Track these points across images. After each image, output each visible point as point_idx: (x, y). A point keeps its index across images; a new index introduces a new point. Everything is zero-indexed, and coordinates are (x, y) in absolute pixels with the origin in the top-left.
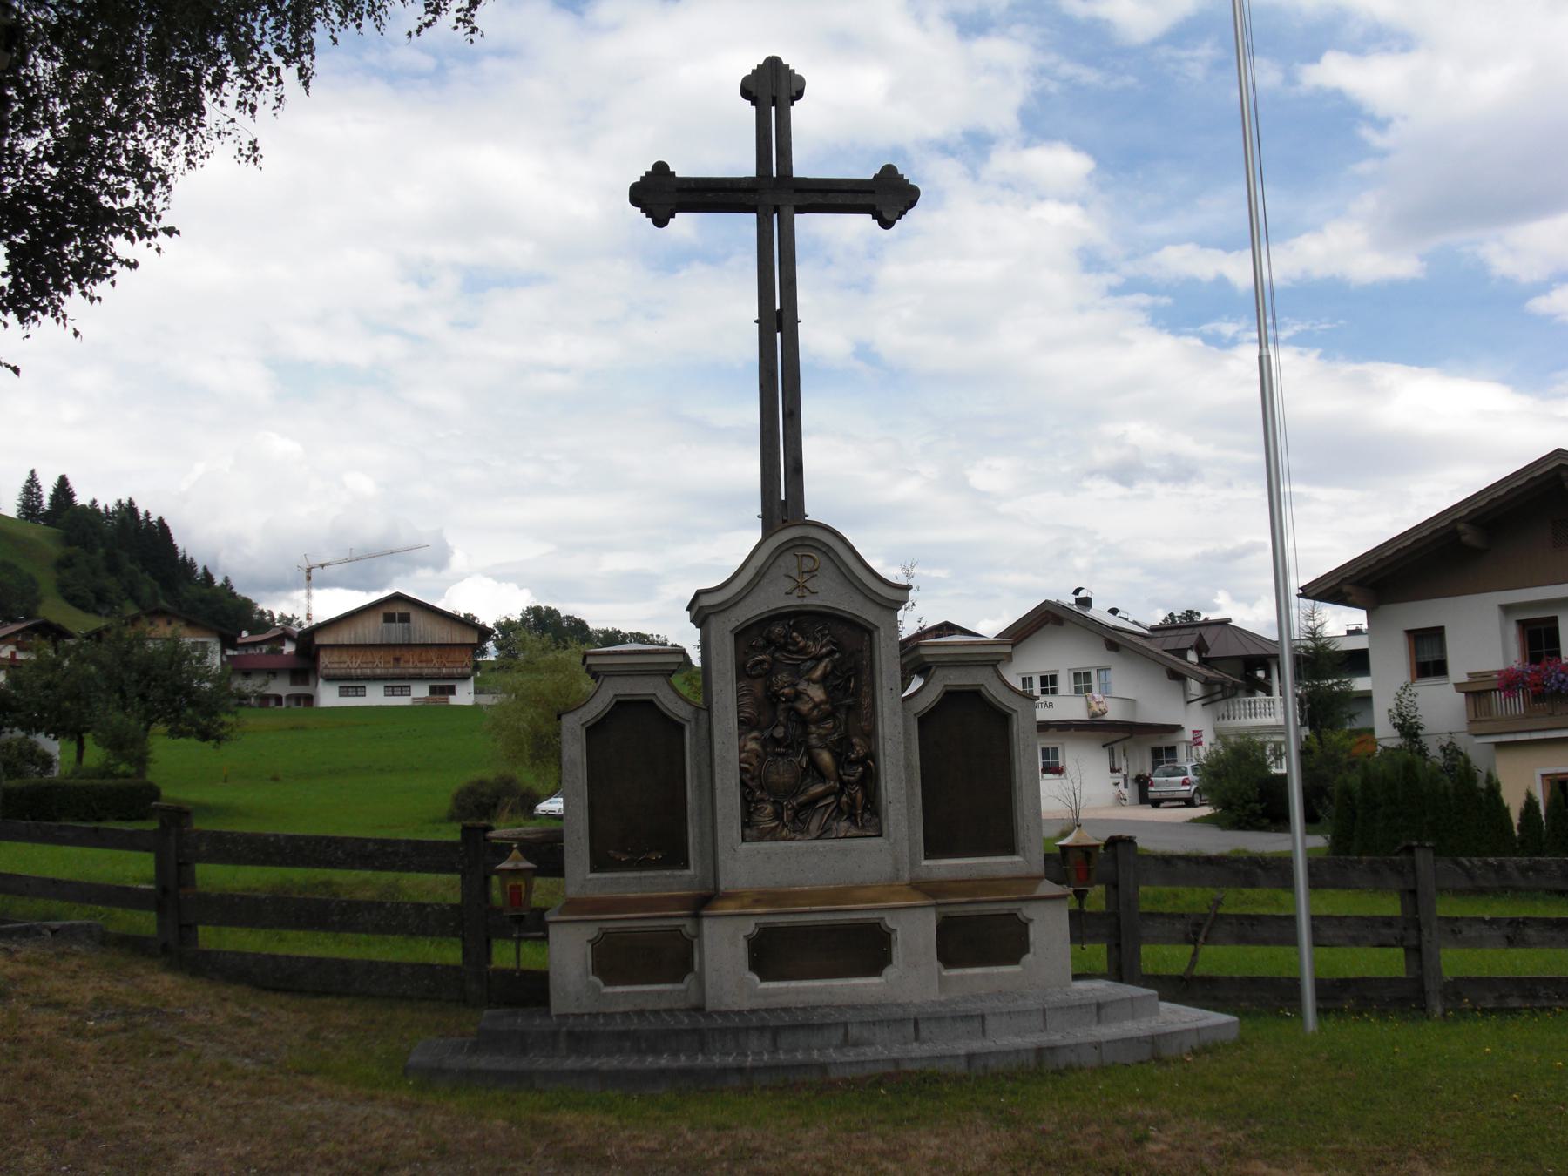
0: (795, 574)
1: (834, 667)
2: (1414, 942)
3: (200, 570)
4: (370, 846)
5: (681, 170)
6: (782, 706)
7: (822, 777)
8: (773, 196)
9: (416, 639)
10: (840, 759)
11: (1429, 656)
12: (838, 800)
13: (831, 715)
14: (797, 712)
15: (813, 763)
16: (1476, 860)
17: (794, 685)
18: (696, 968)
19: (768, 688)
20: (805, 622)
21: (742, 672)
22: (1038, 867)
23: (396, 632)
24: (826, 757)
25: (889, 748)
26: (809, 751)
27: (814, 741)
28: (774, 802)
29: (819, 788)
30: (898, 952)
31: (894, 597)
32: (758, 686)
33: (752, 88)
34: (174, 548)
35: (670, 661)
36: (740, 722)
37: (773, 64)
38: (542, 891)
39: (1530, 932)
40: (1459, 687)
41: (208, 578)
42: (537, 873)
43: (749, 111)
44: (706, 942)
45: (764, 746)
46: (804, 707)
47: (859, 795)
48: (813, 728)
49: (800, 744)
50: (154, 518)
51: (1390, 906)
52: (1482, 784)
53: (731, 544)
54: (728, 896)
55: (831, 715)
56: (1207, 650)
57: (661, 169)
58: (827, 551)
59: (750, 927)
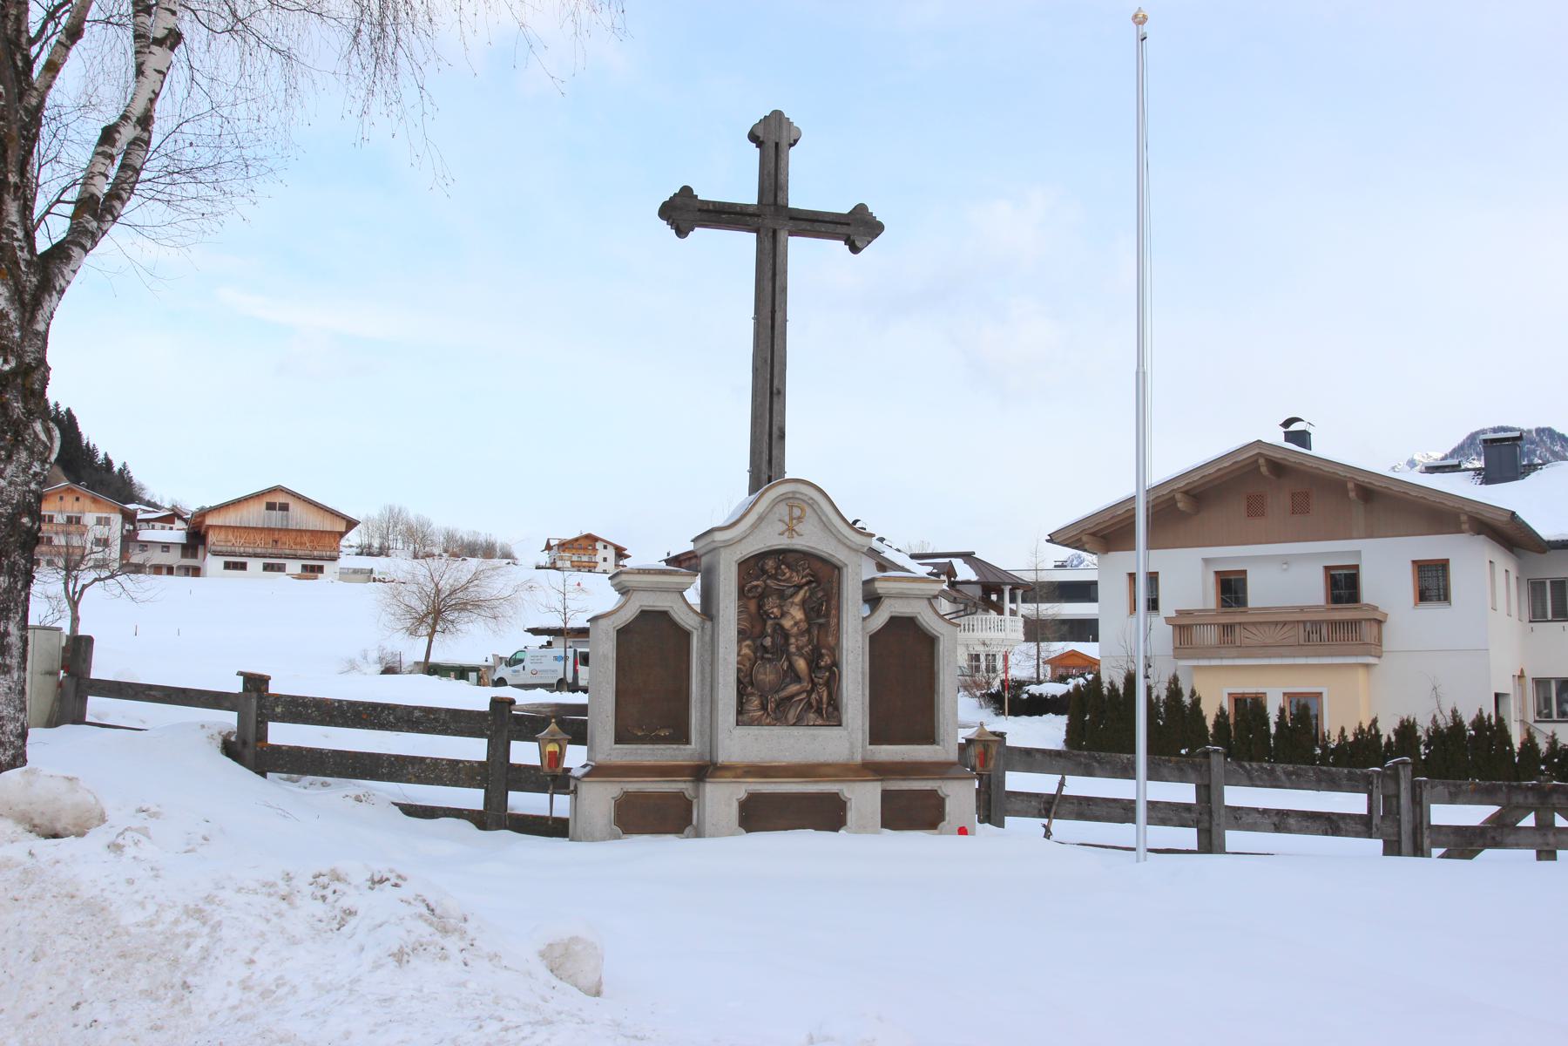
0: (787, 519)
2: (1206, 825)
3: (101, 456)
4: (417, 713)
7: (797, 678)
9: (292, 526)
12: (809, 696)
14: (782, 627)
16: (1255, 765)
18: (695, 822)
21: (742, 593)
23: (275, 519)
24: (801, 664)
25: (851, 658)
27: (793, 649)
29: (794, 688)
32: (753, 606)
33: (760, 133)
34: (79, 435)
36: (739, 632)
37: (777, 116)
39: (1292, 821)
40: (1168, 620)
41: (109, 463)
44: (708, 803)
46: (787, 623)
50: (62, 409)
51: (1184, 793)
52: (1187, 700)
56: (955, 576)
57: (686, 191)
58: (812, 504)
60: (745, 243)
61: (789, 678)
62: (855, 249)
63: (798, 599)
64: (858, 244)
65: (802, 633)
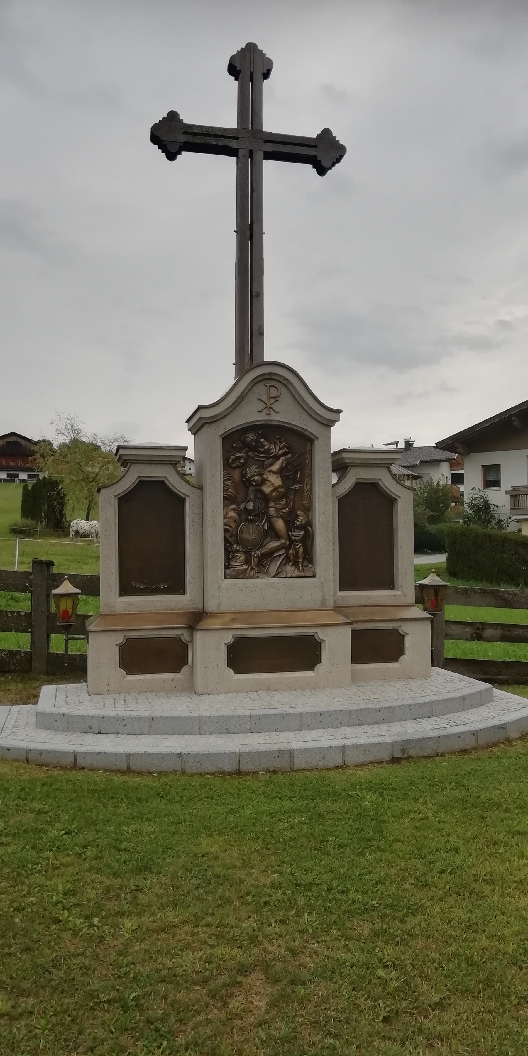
1: (288, 464)
5: (188, 118)
6: (251, 489)
7: (277, 536)
8: (249, 146)
10: (290, 524)
11: (491, 478)
12: (287, 552)
13: (285, 495)
14: (262, 492)
15: (272, 527)
17: (261, 474)
19: (243, 476)
20: (266, 435)
22: (411, 597)
24: (280, 524)
26: (269, 520)
27: (272, 511)
28: (245, 553)
29: (275, 544)
30: (325, 655)
31: (329, 418)
32: (236, 474)
35: (173, 458)
36: (225, 498)
37: (251, 48)
38: (85, 606)
42: (82, 594)
43: (232, 85)
45: (239, 515)
46: (267, 489)
47: (301, 550)
48: (272, 504)
49: (263, 514)
53: (216, 379)
54: (214, 615)
55: (285, 495)
57: (173, 115)
58: (285, 383)
59: (229, 638)
60: (224, 168)
61: (267, 535)
62: (322, 171)
63: (275, 467)
64: (325, 164)
65: (279, 498)
